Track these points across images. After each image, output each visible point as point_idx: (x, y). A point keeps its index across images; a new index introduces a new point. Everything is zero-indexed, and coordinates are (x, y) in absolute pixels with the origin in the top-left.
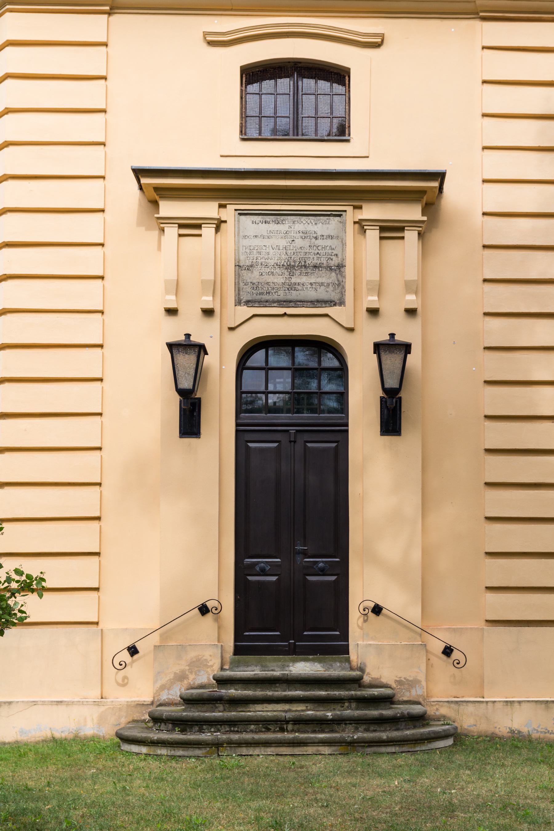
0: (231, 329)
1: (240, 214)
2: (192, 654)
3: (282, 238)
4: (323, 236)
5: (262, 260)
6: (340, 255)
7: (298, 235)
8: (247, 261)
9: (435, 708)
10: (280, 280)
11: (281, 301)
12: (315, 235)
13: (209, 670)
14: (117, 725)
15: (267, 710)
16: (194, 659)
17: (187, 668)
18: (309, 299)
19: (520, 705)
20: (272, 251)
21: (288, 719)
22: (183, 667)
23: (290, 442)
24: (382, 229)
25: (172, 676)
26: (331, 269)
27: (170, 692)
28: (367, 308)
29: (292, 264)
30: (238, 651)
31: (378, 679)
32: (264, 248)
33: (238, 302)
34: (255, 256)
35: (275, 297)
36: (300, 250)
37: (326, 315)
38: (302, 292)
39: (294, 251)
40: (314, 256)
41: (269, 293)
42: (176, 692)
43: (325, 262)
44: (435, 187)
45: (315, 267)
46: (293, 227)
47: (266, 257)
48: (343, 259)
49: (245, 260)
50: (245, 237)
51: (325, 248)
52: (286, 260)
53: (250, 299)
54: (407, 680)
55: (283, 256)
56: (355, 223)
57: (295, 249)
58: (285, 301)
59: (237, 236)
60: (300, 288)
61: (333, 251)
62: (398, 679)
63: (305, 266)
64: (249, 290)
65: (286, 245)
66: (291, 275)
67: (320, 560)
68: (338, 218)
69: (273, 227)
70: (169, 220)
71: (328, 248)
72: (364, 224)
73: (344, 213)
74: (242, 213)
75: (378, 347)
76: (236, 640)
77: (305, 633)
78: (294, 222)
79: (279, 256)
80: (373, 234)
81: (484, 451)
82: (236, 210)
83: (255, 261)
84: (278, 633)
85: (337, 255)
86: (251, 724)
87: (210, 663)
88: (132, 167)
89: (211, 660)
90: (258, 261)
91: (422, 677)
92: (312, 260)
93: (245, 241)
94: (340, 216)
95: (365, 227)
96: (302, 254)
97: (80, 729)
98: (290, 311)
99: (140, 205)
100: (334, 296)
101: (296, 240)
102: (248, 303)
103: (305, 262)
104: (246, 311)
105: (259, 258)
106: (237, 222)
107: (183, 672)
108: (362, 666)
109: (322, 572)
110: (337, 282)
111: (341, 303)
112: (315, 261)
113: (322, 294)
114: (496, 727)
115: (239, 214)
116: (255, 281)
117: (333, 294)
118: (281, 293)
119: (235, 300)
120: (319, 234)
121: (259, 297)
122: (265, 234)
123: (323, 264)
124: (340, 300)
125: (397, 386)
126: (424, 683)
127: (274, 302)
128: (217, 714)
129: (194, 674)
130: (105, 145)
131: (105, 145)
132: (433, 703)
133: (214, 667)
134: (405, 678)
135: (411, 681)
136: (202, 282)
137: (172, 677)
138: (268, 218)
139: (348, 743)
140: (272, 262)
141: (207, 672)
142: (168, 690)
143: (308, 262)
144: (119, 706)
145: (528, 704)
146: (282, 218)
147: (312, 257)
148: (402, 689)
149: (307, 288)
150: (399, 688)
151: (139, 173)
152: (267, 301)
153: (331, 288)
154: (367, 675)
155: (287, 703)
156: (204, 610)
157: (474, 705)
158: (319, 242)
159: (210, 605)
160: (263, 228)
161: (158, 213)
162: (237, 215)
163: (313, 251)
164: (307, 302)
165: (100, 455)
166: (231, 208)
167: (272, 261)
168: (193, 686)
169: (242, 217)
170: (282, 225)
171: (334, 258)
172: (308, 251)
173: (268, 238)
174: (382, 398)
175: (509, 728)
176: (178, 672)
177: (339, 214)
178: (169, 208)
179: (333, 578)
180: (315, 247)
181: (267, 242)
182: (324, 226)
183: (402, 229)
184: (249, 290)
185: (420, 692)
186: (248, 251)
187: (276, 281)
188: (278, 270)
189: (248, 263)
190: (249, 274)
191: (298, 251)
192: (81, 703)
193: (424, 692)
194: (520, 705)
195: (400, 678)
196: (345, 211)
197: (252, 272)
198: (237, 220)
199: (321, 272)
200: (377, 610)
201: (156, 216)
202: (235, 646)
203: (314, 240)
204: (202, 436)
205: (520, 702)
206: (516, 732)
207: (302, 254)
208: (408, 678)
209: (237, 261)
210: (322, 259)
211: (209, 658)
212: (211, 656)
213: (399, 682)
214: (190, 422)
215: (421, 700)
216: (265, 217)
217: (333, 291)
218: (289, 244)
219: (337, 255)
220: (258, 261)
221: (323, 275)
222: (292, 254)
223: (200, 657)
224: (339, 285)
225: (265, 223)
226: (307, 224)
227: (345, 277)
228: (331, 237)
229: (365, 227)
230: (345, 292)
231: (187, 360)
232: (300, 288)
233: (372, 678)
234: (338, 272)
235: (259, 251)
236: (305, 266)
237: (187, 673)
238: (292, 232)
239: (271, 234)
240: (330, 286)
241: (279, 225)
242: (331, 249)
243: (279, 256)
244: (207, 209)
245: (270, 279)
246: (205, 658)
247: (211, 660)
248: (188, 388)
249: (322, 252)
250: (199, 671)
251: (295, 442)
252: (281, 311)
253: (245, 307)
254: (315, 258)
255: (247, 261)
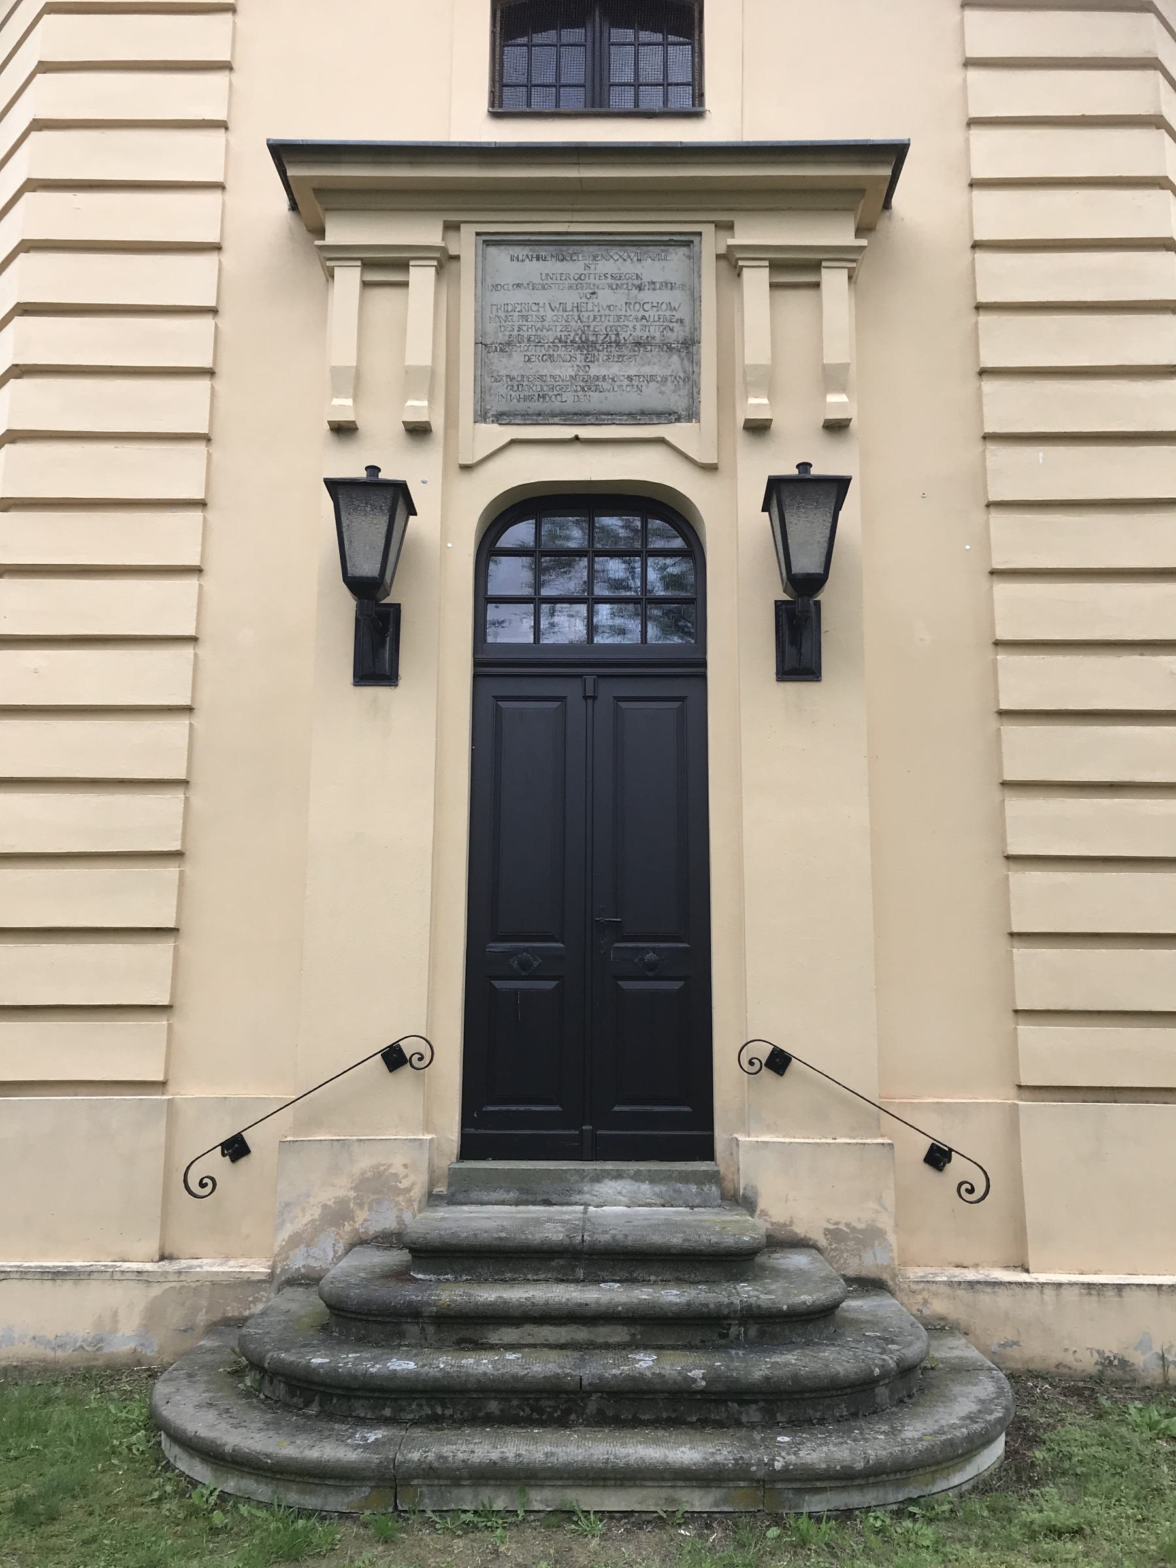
0: (466, 468)
1: (487, 243)
2: (365, 1162)
3: (570, 287)
4: (654, 283)
5: (530, 332)
6: (687, 322)
7: (604, 281)
8: (500, 334)
9: (919, 1298)
10: (566, 370)
11: (569, 414)
12: (637, 282)
13: (401, 1198)
14: (185, 1331)
15: (531, 1341)
16: (369, 1174)
17: (352, 1194)
18: (626, 408)
19: (1120, 1296)
20: (550, 314)
21: (588, 1388)
22: (341, 1193)
23: (585, 698)
24: (776, 266)
25: (316, 1212)
26: (670, 349)
27: (311, 1252)
28: (747, 421)
29: (592, 338)
30: (470, 1148)
31: (785, 1225)
32: (535, 308)
33: (482, 416)
34: (517, 324)
35: (557, 405)
36: (607, 312)
37: (661, 441)
38: (610, 395)
39: (596, 313)
40: (635, 323)
41: (544, 397)
42: (324, 1251)
43: (658, 335)
44: (884, 177)
45: (638, 344)
46: (592, 267)
47: (539, 325)
48: (695, 329)
49: (496, 333)
50: (496, 287)
51: (657, 306)
52: (580, 332)
53: (505, 408)
54: (854, 1229)
55: (573, 324)
56: (719, 257)
57: (596, 309)
58: (575, 414)
59: (479, 285)
60: (606, 385)
61: (674, 313)
62: (831, 1227)
63: (618, 344)
64: (503, 391)
65: (579, 301)
66: (589, 360)
67: (646, 945)
68: (685, 249)
69: (553, 266)
70: (344, 253)
71: (664, 306)
72: (738, 256)
73: (696, 239)
74: (490, 241)
75: (777, 488)
76: (465, 1123)
77: (616, 1109)
78: (595, 258)
79: (564, 323)
80: (756, 279)
81: (996, 715)
82: (478, 234)
83: (515, 333)
84: (558, 1108)
85: (681, 321)
86: (489, 1398)
87: (405, 1184)
88: (268, 140)
89: (406, 1176)
90: (521, 333)
91: (885, 1222)
92: (632, 330)
93: (496, 294)
94: (688, 244)
95: (741, 263)
96: (611, 319)
97: (101, 1340)
98: (585, 432)
99: (290, 229)
100: (678, 402)
101: (600, 292)
102: (501, 418)
103: (617, 335)
104: (497, 434)
105: (525, 328)
106: (480, 258)
107: (342, 1202)
108: (750, 1194)
109: (653, 971)
110: (682, 375)
111: (692, 415)
112: (638, 333)
113: (652, 398)
114: (1066, 1350)
115: (484, 241)
116: (514, 374)
117: (674, 398)
118: (568, 396)
119: (475, 411)
120: (646, 279)
121: (522, 406)
122: (537, 281)
123: (653, 338)
124: (688, 409)
125: (821, 571)
126: (892, 1238)
127: (553, 415)
128: (402, 1365)
129: (366, 1208)
130: (227, 128)
131: (227, 128)
132: (914, 1287)
133: (412, 1194)
134: (847, 1225)
135: (862, 1231)
136: (407, 372)
137: (316, 1217)
138: (543, 251)
139: (758, 1481)
140: (550, 335)
141: (398, 1204)
142: (308, 1246)
143: (623, 335)
144: (194, 1285)
145: (1140, 1293)
146: (572, 249)
147: (630, 325)
148: (842, 1252)
149: (619, 386)
150: (835, 1249)
151: (282, 153)
152: (539, 415)
153: (670, 385)
154: (760, 1215)
155: (584, 1325)
156: (394, 1058)
157: (1010, 1292)
158: (647, 296)
159: (408, 1048)
160: (533, 270)
161: (324, 239)
162: (480, 246)
163: (634, 314)
164: (621, 414)
165: (187, 722)
166: (468, 234)
167: (550, 333)
168: (364, 1237)
169: (492, 250)
170: (571, 263)
171: (676, 326)
172: (623, 313)
173: (544, 288)
174: (778, 604)
175: (1098, 1352)
176: (330, 1203)
177: (687, 242)
178: (342, 232)
179: (677, 985)
180: (637, 306)
181: (541, 297)
182: (657, 263)
183: (816, 266)
184: (503, 391)
185: (883, 1260)
186: (502, 314)
187: (557, 372)
188: (562, 352)
189: (502, 338)
190: (504, 360)
191: (602, 313)
192: (113, 1276)
193: (893, 1259)
194: (1120, 1296)
195: (837, 1223)
196: (700, 234)
197: (510, 355)
198: (480, 252)
199: (649, 355)
200: (779, 1061)
201: (318, 243)
202: (464, 1137)
203: (635, 292)
204: (400, 682)
205: (1119, 1288)
206: (1116, 1362)
207: (611, 319)
208: (854, 1224)
209: (480, 333)
210: (652, 329)
211: (401, 1171)
212: (405, 1166)
213: (834, 1234)
214: (377, 653)
215: (885, 1276)
216: (537, 248)
217: (674, 391)
218: (585, 300)
219: (681, 321)
220: (521, 333)
221: (655, 360)
222: (592, 318)
223: (382, 1168)
224: (687, 379)
225: (538, 259)
226: (621, 260)
227: (699, 364)
228: (668, 285)
229: (741, 263)
230: (699, 393)
231: (370, 527)
232: (606, 385)
233: (772, 1224)
234: (683, 354)
235: (524, 313)
236: (618, 344)
237: (352, 1205)
238: (592, 276)
239: (550, 281)
240: (669, 383)
241: (565, 263)
242: (671, 310)
243: (564, 323)
244: (424, 232)
245: (547, 369)
246: (392, 1171)
247: (406, 1176)
248: (369, 574)
249: (652, 313)
250: (379, 1202)
251: (594, 698)
252: (568, 432)
253: (496, 425)
254: (638, 328)
255: (500, 334)
